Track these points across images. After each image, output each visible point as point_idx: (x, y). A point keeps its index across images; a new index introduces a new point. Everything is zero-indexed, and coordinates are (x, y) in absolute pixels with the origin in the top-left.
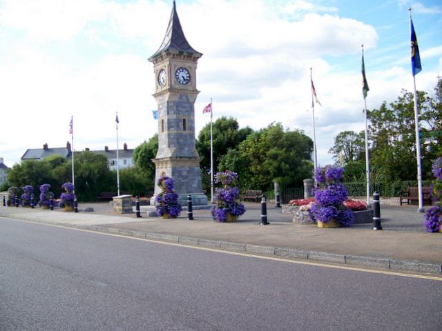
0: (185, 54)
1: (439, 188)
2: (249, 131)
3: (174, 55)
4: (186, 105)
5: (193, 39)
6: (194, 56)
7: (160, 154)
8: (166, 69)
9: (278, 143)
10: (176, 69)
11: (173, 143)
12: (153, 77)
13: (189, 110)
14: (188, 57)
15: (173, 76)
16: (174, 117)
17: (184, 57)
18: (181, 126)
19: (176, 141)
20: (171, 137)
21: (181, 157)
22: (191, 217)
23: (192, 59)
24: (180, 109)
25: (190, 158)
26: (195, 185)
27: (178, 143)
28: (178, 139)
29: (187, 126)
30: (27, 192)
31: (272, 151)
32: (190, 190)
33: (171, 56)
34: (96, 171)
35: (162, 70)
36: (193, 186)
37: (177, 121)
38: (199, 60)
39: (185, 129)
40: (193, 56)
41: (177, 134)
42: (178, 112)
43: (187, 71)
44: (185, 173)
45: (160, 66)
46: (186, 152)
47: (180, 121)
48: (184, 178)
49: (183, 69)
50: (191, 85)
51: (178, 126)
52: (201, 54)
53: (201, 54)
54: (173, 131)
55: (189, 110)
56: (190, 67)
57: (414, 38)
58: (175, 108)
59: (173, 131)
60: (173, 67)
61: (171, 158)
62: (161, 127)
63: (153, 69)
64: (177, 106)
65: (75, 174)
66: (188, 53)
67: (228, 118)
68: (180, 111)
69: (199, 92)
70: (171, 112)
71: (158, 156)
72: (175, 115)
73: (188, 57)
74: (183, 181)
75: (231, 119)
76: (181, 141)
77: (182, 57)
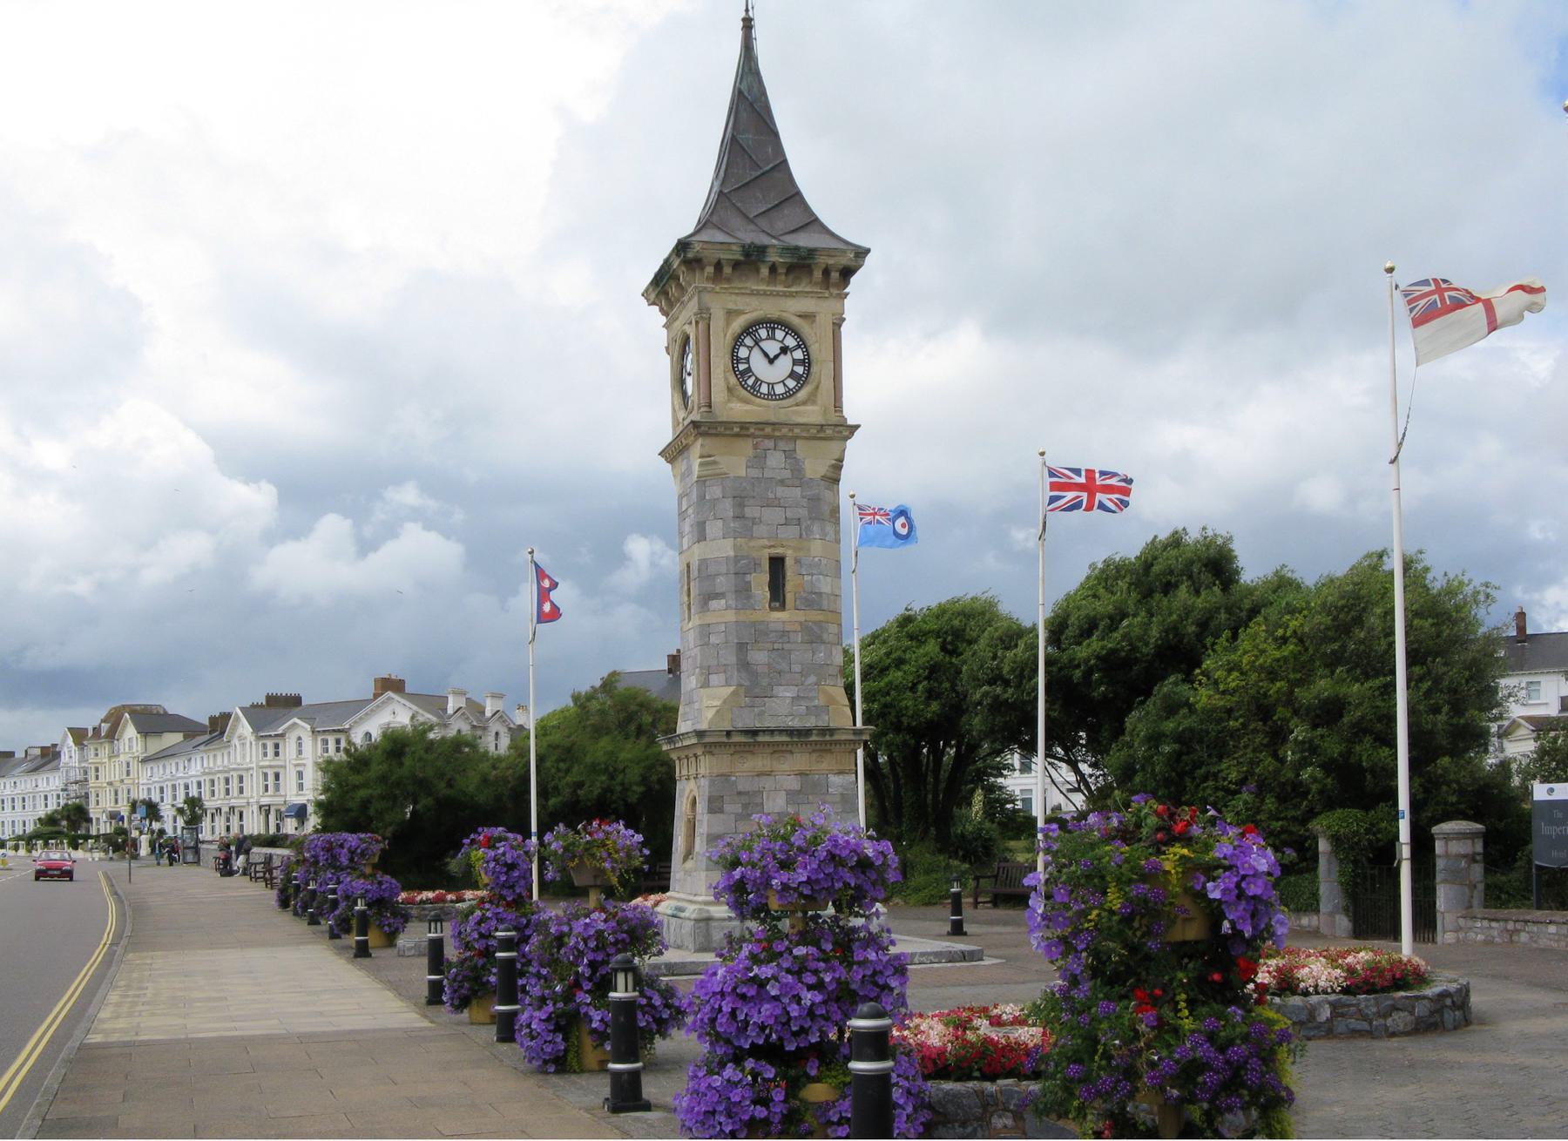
2: (1282, 583)
3: (718, 266)
4: (781, 491)
5: (825, 172)
6: (823, 260)
9: (434, 719)
10: (738, 324)
11: (724, 668)
13: (803, 513)
14: (790, 269)
16: (721, 548)
17: (773, 269)
18: (761, 590)
20: (714, 639)
21: (754, 733)
23: (818, 274)
25: (800, 735)
27: (744, 665)
28: (742, 647)
29: (790, 586)
31: (1323, 686)
33: (710, 270)
34: (634, 774)
37: (741, 569)
42: (743, 524)
43: (796, 334)
46: (783, 709)
47: (756, 565)
49: (772, 324)
50: (811, 399)
51: (743, 591)
53: (862, 253)
54: (723, 613)
55: (803, 513)
56: (808, 317)
58: (727, 508)
59: (723, 613)
60: (717, 323)
64: (740, 501)
65: (543, 794)
67: (1193, 535)
68: (755, 521)
69: (857, 427)
70: (715, 528)
72: (729, 542)
73: (790, 269)
75: (1208, 543)
76: (759, 657)
77: (765, 271)
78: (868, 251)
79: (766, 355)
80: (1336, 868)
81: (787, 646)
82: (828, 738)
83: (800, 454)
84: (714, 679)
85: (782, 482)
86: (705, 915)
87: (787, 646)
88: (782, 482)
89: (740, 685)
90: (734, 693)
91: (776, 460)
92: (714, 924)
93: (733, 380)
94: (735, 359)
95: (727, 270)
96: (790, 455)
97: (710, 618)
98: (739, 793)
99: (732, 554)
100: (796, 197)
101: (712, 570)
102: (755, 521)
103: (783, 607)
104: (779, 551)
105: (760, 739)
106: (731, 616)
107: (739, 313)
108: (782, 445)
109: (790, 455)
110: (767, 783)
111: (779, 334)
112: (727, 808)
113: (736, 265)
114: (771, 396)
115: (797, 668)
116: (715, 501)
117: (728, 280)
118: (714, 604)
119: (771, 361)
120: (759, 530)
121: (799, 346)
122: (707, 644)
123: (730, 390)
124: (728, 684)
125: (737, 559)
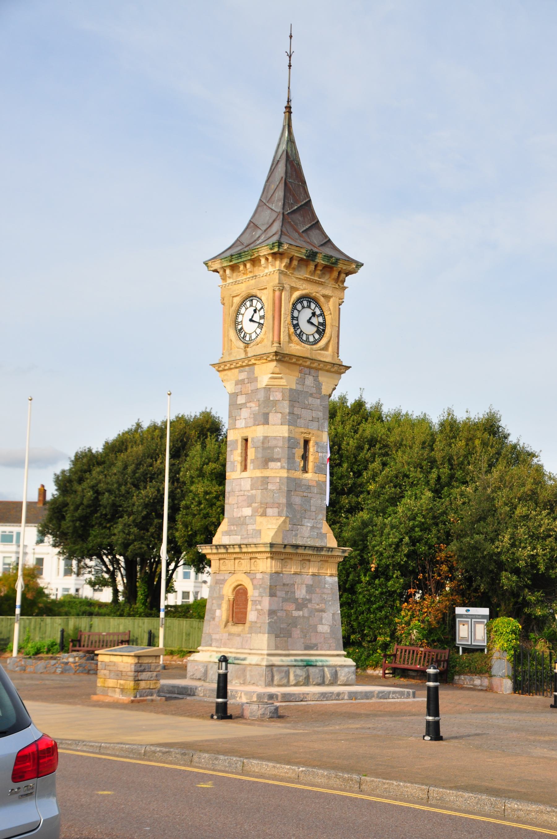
0: (320, 260)
1: (402, 838)
6: (340, 266)
7: (228, 533)
8: (266, 296)
12: (216, 317)
15: (286, 319)
19: (284, 500)
20: (270, 487)
21: (297, 547)
22: (434, 731)
23: (335, 274)
24: (297, 411)
26: (324, 628)
27: (289, 505)
28: (289, 491)
30: (400, 584)
32: (314, 641)
33: (286, 261)
35: (250, 297)
36: (320, 628)
38: (349, 280)
39: (305, 470)
40: (335, 267)
41: (288, 478)
44: (301, 593)
45: (243, 282)
48: (300, 606)
52: (359, 265)
53: (359, 265)
56: (324, 296)
57: (289, 110)
58: (285, 407)
61: (272, 545)
62: (244, 451)
63: (217, 294)
66: (328, 257)
68: (299, 417)
70: (275, 418)
71: (219, 538)
72: (286, 428)
74: (296, 614)
76: (297, 500)
77: (312, 267)
78: (362, 265)
79: (252, 317)
80: (121, 701)
81: (309, 495)
82: (330, 554)
83: (320, 379)
84: (270, 511)
85: (311, 395)
86: (271, 663)
87: (309, 495)
88: (311, 395)
89: (287, 517)
90: (284, 522)
91: (309, 381)
92: (275, 669)
93: (292, 330)
94: (293, 318)
95: (295, 263)
96: (316, 378)
97: (267, 473)
98: (284, 585)
99: (286, 435)
100: (317, 225)
101: (272, 443)
102: (299, 417)
103: (307, 472)
104: (307, 436)
105: (300, 551)
106: (284, 474)
107: (297, 289)
108: (313, 371)
109: (316, 378)
110: (298, 579)
111: (313, 306)
112: (279, 593)
113: (301, 260)
114: (307, 341)
115: (313, 509)
116: (275, 402)
117: (294, 269)
118: (272, 465)
119: (251, 320)
120: (301, 422)
121: (321, 315)
122: (266, 489)
123: (289, 336)
124: (280, 515)
125: (289, 438)
